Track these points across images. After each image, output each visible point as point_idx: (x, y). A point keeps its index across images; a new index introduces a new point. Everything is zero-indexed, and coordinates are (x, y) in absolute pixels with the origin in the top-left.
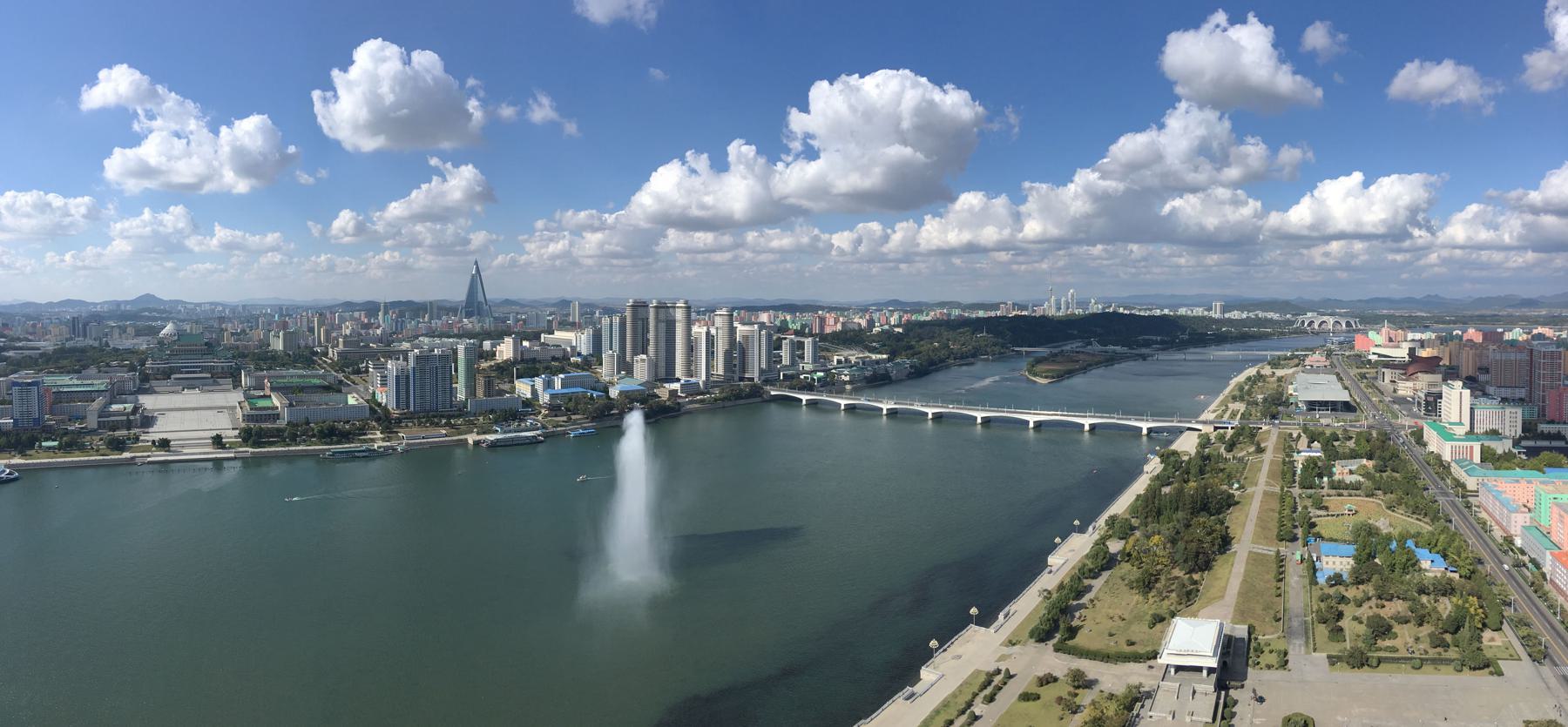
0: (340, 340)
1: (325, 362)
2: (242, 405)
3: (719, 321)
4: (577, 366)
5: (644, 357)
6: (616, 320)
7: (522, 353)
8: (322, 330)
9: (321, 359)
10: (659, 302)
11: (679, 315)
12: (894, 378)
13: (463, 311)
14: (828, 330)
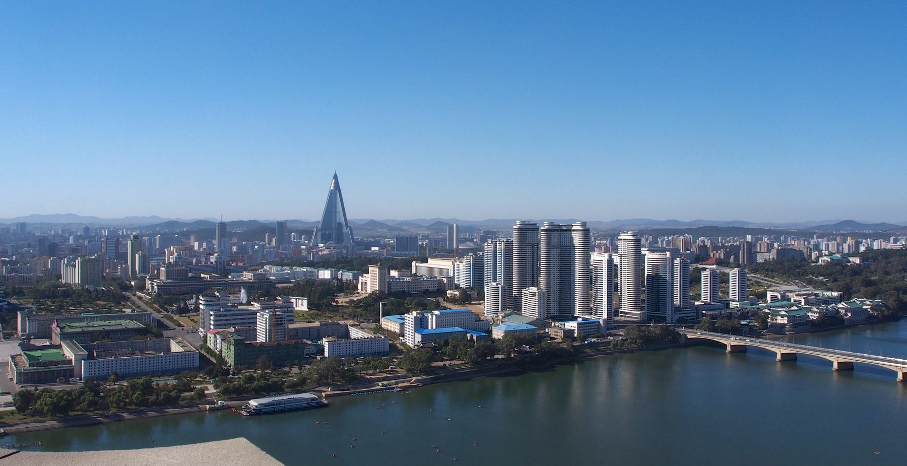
0: (162, 269)
1: (140, 298)
2: (18, 359)
3: (623, 247)
4: (454, 300)
5: (534, 289)
6: (501, 247)
7: (389, 283)
8: (137, 256)
9: (135, 295)
10: (551, 224)
11: (577, 239)
12: (846, 323)
13: (319, 234)
14: (760, 259)
